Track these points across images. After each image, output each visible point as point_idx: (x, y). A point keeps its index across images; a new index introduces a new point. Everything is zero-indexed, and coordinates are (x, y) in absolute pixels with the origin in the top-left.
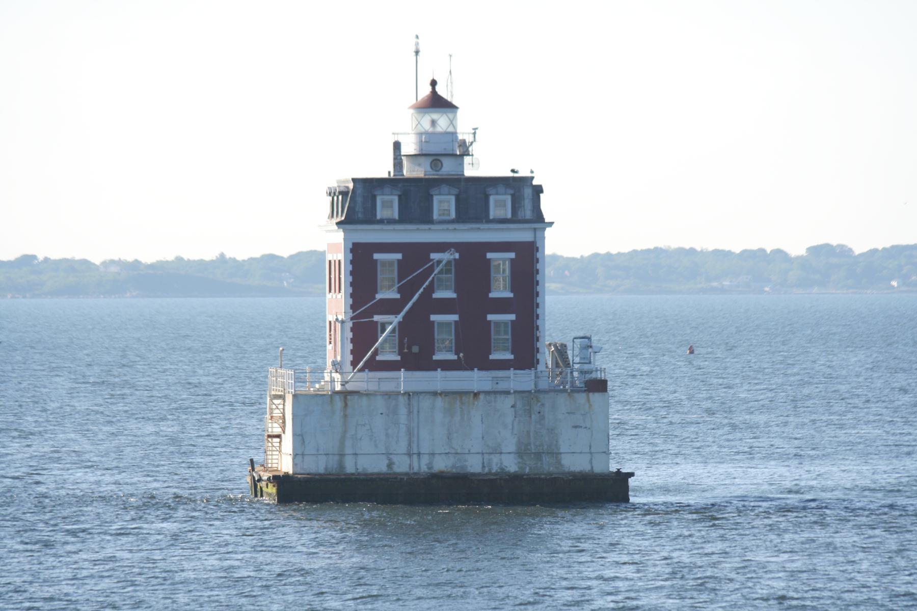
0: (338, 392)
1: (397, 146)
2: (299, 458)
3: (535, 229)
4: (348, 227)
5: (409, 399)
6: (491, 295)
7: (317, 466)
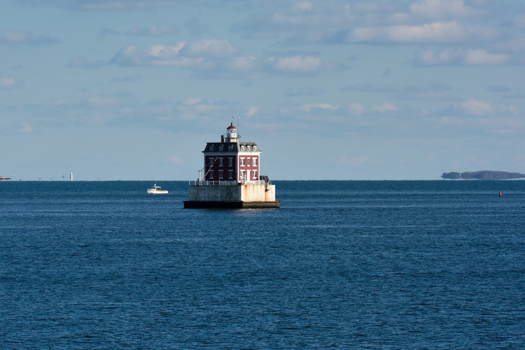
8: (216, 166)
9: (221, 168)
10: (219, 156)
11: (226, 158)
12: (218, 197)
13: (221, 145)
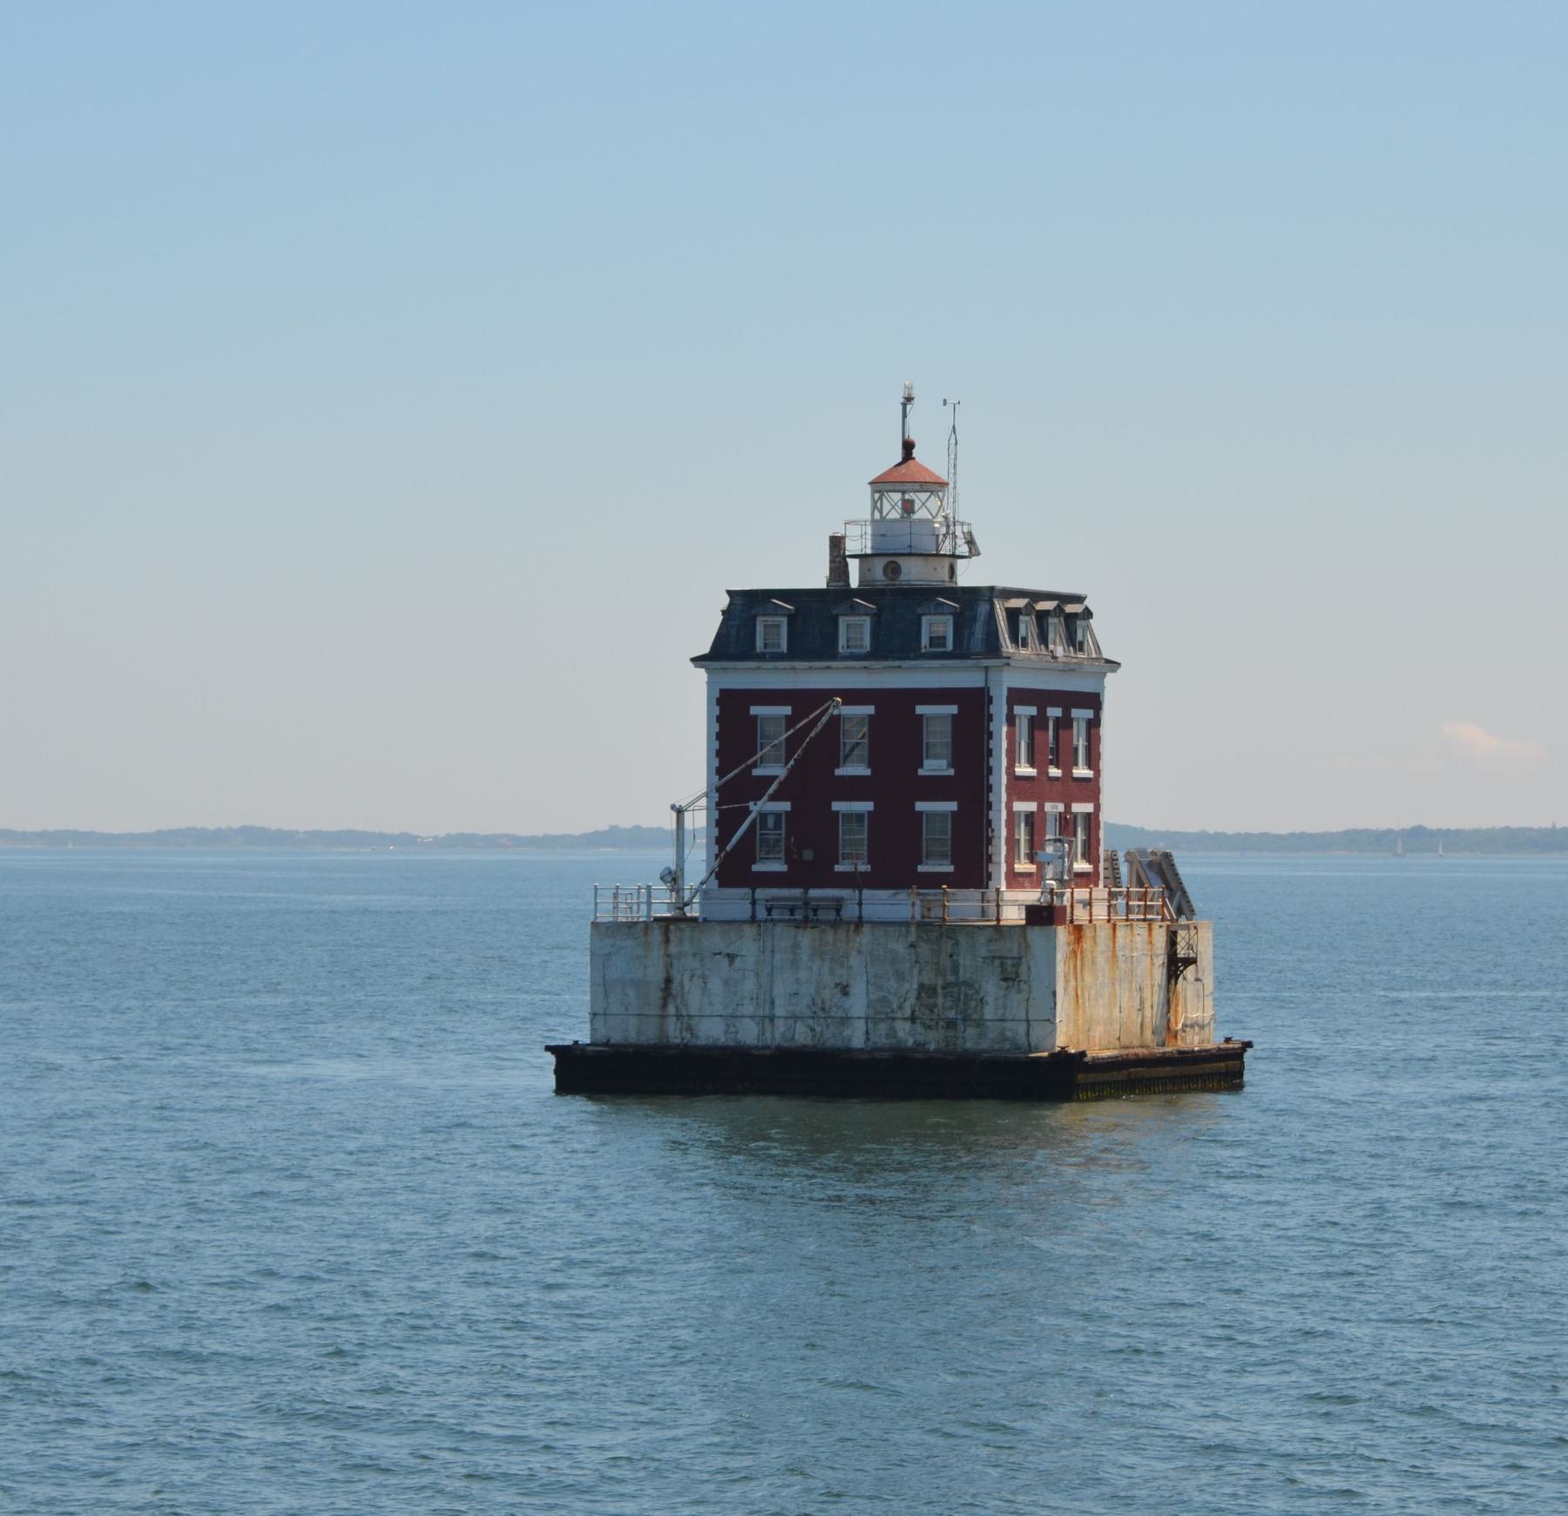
0: (657, 919)
1: (836, 543)
2: (600, 1021)
3: (986, 668)
4: (718, 665)
5: (1150, 930)
6: (921, 772)
7: (629, 1031)
8: (813, 779)
9: (853, 789)
10: (852, 697)
11: (895, 714)
12: (845, 1020)
13: (854, 610)
